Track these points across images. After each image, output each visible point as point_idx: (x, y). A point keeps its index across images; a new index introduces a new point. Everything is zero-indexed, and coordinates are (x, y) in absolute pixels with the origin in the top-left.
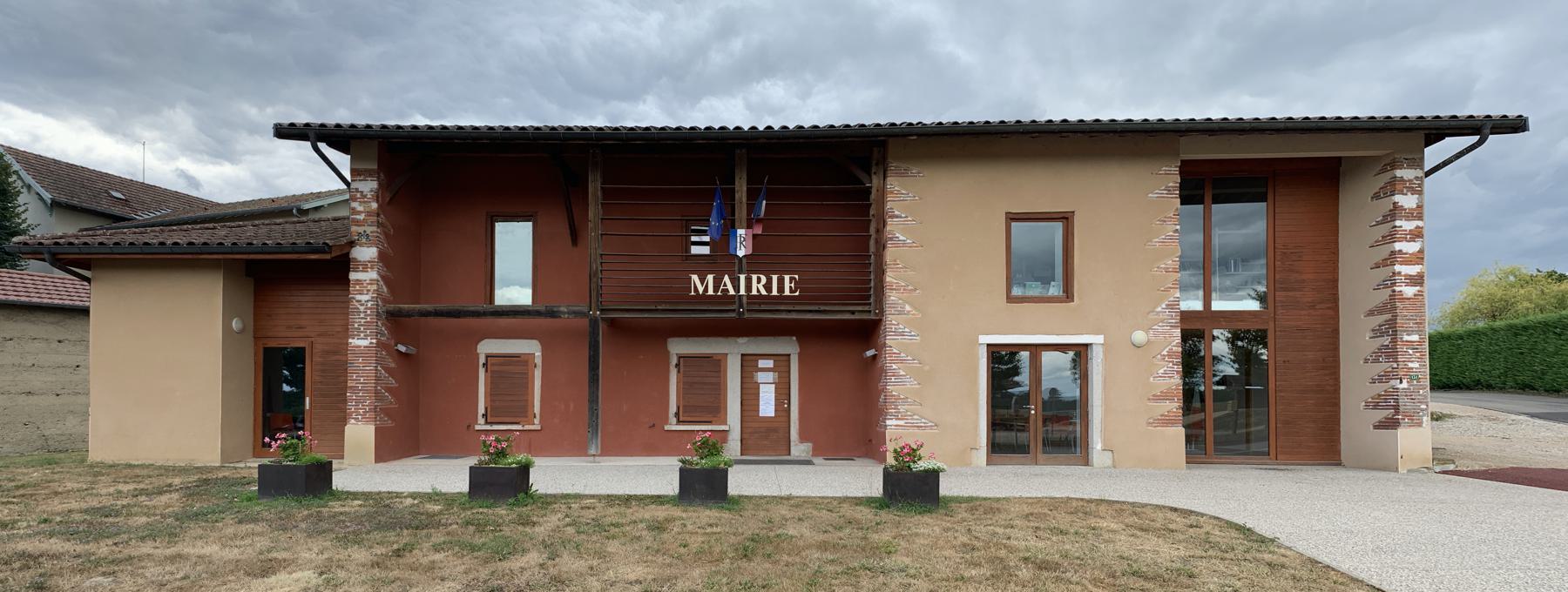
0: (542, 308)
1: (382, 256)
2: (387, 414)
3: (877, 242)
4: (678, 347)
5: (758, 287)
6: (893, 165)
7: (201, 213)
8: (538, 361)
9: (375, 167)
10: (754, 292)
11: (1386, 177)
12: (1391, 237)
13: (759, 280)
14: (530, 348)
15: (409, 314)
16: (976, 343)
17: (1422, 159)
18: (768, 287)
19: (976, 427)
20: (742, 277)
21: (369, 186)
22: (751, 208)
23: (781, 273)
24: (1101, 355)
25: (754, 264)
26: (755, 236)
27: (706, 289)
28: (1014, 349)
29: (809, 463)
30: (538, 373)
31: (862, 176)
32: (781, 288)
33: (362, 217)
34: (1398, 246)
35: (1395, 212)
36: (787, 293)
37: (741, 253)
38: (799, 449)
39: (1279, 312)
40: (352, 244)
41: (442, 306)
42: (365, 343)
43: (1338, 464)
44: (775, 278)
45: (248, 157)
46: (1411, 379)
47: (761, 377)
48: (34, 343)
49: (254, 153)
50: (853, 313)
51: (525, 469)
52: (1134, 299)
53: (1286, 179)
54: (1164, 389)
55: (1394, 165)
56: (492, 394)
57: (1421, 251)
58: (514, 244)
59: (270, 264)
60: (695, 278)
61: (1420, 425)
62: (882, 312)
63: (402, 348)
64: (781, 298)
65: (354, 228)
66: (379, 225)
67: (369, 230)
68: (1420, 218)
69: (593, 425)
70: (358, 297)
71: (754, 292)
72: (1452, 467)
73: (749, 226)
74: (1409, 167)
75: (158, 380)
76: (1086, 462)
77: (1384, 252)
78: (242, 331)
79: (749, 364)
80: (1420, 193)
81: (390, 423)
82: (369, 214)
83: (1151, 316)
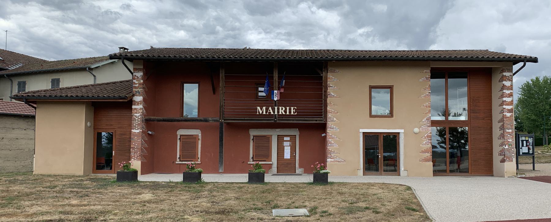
1: (144, 99)
3: (325, 95)
4: (253, 133)
5: (282, 111)
6: (330, 69)
7: (40, 69)
8: (200, 137)
9: (142, 67)
10: (280, 113)
12: (502, 96)
13: (282, 109)
14: (197, 132)
15: (153, 120)
18: (285, 112)
20: (276, 108)
21: (140, 74)
22: (279, 83)
23: (290, 107)
25: (280, 103)
26: (281, 93)
28: (376, 135)
29: (300, 175)
30: (200, 142)
31: (320, 72)
32: (290, 112)
33: (137, 85)
34: (504, 99)
35: (504, 87)
36: (292, 113)
37: (275, 99)
38: (298, 171)
40: (133, 95)
41: (165, 118)
42: (138, 131)
43: (493, 176)
44: (288, 108)
45: (13, 16)
46: (509, 145)
47: (285, 144)
48: (16, 132)
49: (17, 13)
50: (316, 120)
51: (200, 173)
52: (416, 117)
53: (479, 70)
54: (425, 149)
55: (503, 71)
57: (512, 101)
58: (191, 94)
59: (104, 106)
61: (512, 161)
62: (326, 120)
63: (150, 133)
64: (290, 115)
65: (134, 90)
66: (143, 88)
67: (140, 90)
68: (512, 89)
70: (135, 115)
71: (280, 113)
72: (524, 176)
73: (279, 89)
74: (508, 72)
75: (60, 144)
76: (399, 175)
77: (500, 101)
78: (90, 127)
79: (280, 139)
80: (512, 81)
81: (145, 161)
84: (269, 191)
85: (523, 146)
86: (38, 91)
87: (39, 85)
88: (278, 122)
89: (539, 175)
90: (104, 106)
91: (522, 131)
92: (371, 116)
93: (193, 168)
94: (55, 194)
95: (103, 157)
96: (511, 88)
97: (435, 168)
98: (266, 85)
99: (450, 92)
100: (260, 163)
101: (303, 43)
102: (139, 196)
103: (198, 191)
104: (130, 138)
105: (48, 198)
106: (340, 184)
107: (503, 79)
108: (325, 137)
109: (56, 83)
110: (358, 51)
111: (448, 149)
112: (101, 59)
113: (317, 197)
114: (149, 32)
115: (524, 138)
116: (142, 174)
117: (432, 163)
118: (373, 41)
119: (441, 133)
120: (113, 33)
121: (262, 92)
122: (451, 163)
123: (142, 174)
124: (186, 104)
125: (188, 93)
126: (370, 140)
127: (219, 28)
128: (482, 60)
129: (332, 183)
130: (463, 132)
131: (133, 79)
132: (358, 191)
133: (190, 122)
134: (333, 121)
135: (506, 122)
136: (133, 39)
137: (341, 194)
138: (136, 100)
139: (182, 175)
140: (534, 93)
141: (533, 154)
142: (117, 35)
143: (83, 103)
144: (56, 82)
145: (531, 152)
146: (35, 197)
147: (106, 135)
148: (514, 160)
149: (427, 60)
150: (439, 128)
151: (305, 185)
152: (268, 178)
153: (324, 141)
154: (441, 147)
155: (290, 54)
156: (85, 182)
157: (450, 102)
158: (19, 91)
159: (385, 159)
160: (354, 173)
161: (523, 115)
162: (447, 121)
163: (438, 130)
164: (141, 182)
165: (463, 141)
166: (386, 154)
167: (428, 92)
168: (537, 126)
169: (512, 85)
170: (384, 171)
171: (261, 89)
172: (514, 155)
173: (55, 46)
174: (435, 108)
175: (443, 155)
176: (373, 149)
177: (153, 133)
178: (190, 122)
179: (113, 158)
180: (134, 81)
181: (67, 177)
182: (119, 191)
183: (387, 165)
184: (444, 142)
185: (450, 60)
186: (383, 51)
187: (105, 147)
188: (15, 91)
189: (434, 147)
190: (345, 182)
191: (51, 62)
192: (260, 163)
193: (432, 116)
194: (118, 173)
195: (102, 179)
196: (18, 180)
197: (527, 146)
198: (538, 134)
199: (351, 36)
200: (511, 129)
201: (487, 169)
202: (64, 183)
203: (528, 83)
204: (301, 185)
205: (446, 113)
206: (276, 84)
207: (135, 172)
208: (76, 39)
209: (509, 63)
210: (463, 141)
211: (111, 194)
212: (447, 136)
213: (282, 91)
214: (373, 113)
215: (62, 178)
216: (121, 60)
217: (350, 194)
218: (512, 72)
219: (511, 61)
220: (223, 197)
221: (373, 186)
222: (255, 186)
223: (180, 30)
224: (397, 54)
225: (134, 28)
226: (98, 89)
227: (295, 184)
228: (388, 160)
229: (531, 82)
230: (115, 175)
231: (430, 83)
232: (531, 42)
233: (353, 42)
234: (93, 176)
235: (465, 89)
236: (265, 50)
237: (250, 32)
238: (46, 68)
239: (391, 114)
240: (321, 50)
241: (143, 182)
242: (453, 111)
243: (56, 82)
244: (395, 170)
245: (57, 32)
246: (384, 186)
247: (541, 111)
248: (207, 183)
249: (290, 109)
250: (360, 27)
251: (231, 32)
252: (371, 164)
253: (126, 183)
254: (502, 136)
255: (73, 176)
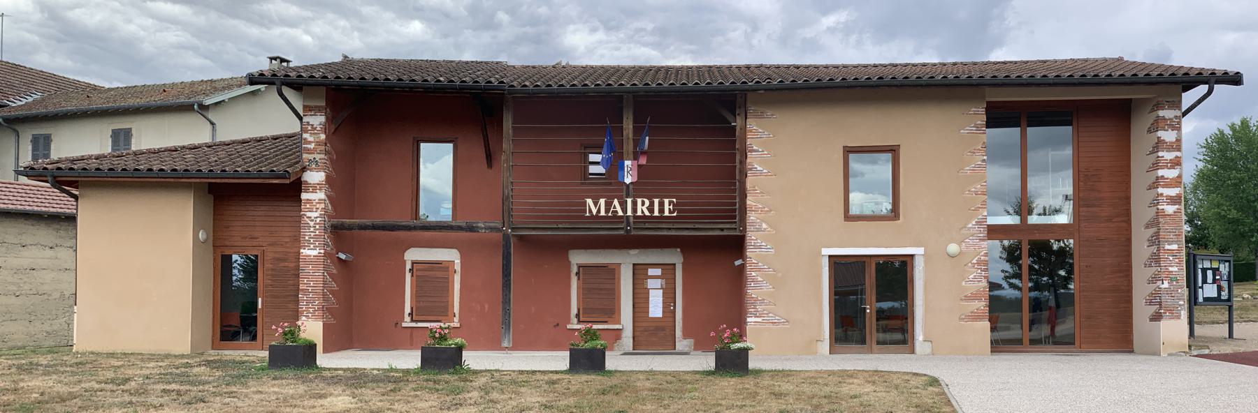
0: (462, 223)
1: (329, 179)
2: (331, 314)
4: (578, 258)
5: (642, 209)
6: (751, 109)
7: (85, 105)
8: (458, 267)
9: (323, 104)
10: (639, 213)
11: (1153, 115)
12: (1156, 166)
13: (643, 204)
14: (451, 256)
15: (350, 228)
16: (820, 255)
17: (1180, 101)
18: (651, 209)
19: (821, 323)
20: (629, 201)
21: (318, 120)
22: (637, 143)
23: (662, 198)
24: (922, 264)
25: (638, 190)
27: (599, 211)
31: (729, 117)
32: (661, 210)
34: (1160, 173)
35: (1159, 145)
36: (667, 213)
37: (628, 180)
38: (682, 344)
39: (1083, 225)
40: (304, 169)
41: (378, 221)
42: (315, 253)
43: (1131, 351)
44: (656, 201)
47: (651, 283)
48: (33, 252)
50: (722, 230)
51: (460, 349)
53: (1102, 107)
54: (973, 291)
55: (1158, 106)
56: (417, 296)
57: (1180, 176)
58: (437, 167)
59: (238, 193)
60: (589, 201)
61: (1179, 317)
63: (343, 256)
64: (662, 218)
66: (327, 153)
67: (318, 157)
68: (1179, 149)
69: (506, 323)
70: (309, 214)
71: (639, 213)
72: (1207, 352)
73: (635, 158)
74: (1170, 108)
75: (136, 278)
78: (205, 242)
80: (1179, 129)
81: (332, 321)
82: (318, 143)
83: (964, 231)
84: (615, 390)
85: (1205, 281)
86: (82, 159)
87: (81, 143)
88: (633, 233)
89: (1242, 350)
90: (238, 193)
91: (1206, 247)
92: (848, 217)
93: (443, 338)
94: (127, 398)
95: (236, 311)
96: (1177, 146)
97: (996, 334)
98: (605, 148)
99: (1032, 157)
100: (595, 327)
101: (692, 52)
102: (321, 402)
103: (456, 391)
104: (297, 268)
105: (110, 406)
106: (775, 373)
107: (1157, 124)
108: (743, 267)
109: (122, 138)
110: (816, 67)
111: (1025, 290)
112: (228, 85)
113: (723, 402)
114: (342, 23)
115: (1207, 264)
116: (326, 350)
117: (988, 324)
118: (859, 42)
119: (1012, 255)
120: (261, 25)
121: (597, 164)
122: (1032, 323)
123: (326, 350)
124: (426, 190)
125: (428, 165)
126: (846, 273)
127: (502, 16)
128: (1109, 82)
129: (758, 372)
130: (1063, 252)
131: (303, 130)
132: (816, 389)
133: (436, 232)
134: (759, 230)
135: (1165, 225)
136: (307, 39)
137: (778, 395)
138: (310, 181)
139: (418, 353)
140: (1236, 158)
141: (1229, 300)
142: (269, 29)
143: (187, 186)
144: (122, 138)
145: (1225, 295)
146: (80, 403)
147: (240, 261)
148: (1184, 314)
149: (978, 85)
150: (1006, 243)
151: (698, 376)
152: (613, 361)
153: (739, 277)
154: (1012, 286)
155: (661, 75)
156: (196, 370)
157: (1032, 184)
158: (35, 158)
159: (881, 315)
160: (809, 349)
161: (1209, 209)
162: (1024, 227)
163: (1004, 248)
164: (325, 369)
165: (1062, 273)
166: (886, 305)
167: (979, 158)
168: (1243, 235)
169: (1179, 140)
170: (878, 343)
171: (593, 157)
172: (1183, 303)
173: (125, 51)
174: (996, 195)
175: (1015, 305)
176: (855, 293)
177: (350, 258)
178: (436, 232)
179: (259, 316)
180: (305, 136)
181: (152, 357)
182: (276, 389)
183: (885, 330)
184: (1018, 276)
185: (1032, 83)
186: (875, 66)
187: (238, 287)
188: (26, 159)
189: (993, 286)
190: (787, 368)
191: (110, 90)
192: (595, 327)
193: (990, 214)
194: (272, 349)
195: (234, 362)
196: (37, 365)
197: (1214, 281)
198: (1244, 254)
199: (808, 33)
200: (1177, 242)
201: (1118, 335)
202: (148, 372)
203: (1222, 133)
204: (688, 377)
205: (1024, 208)
206: (629, 147)
207: (311, 348)
208: (173, 36)
209: (1174, 86)
210: (1062, 273)
211: (257, 397)
212: (1026, 261)
213: (643, 161)
214: (854, 210)
215: (142, 360)
216: (274, 88)
217: (799, 396)
218: (1179, 108)
219: (1176, 83)
220: (514, 404)
221: (851, 377)
222: (584, 377)
223: (413, 18)
224: (907, 72)
225: (307, 14)
226: (222, 154)
227: (674, 374)
228: (888, 318)
229: (1228, 131)
230: (266, 354)
231: (984, 138)
232: (1230, 38)
233: (812, 45)
234: (213, 355)
235: (1068, 152)
236: (602, 67)
237: (572, 27)
238: (98, 103)
239: (895, 213)
240: (731, 67)
241: (329, 369)
242: (1039, 204)
243: (122, 138)
244: (904, 342)
245: (130, 21)
246: (876, 376)
247: (1252, 198)
248: (476, 372)
249: (661, 204)
250: (825, 12)
251: (528, 29)
252: (848, 327)
253: (289, 373)
254: (1156, 259)
255: (167, 356)
